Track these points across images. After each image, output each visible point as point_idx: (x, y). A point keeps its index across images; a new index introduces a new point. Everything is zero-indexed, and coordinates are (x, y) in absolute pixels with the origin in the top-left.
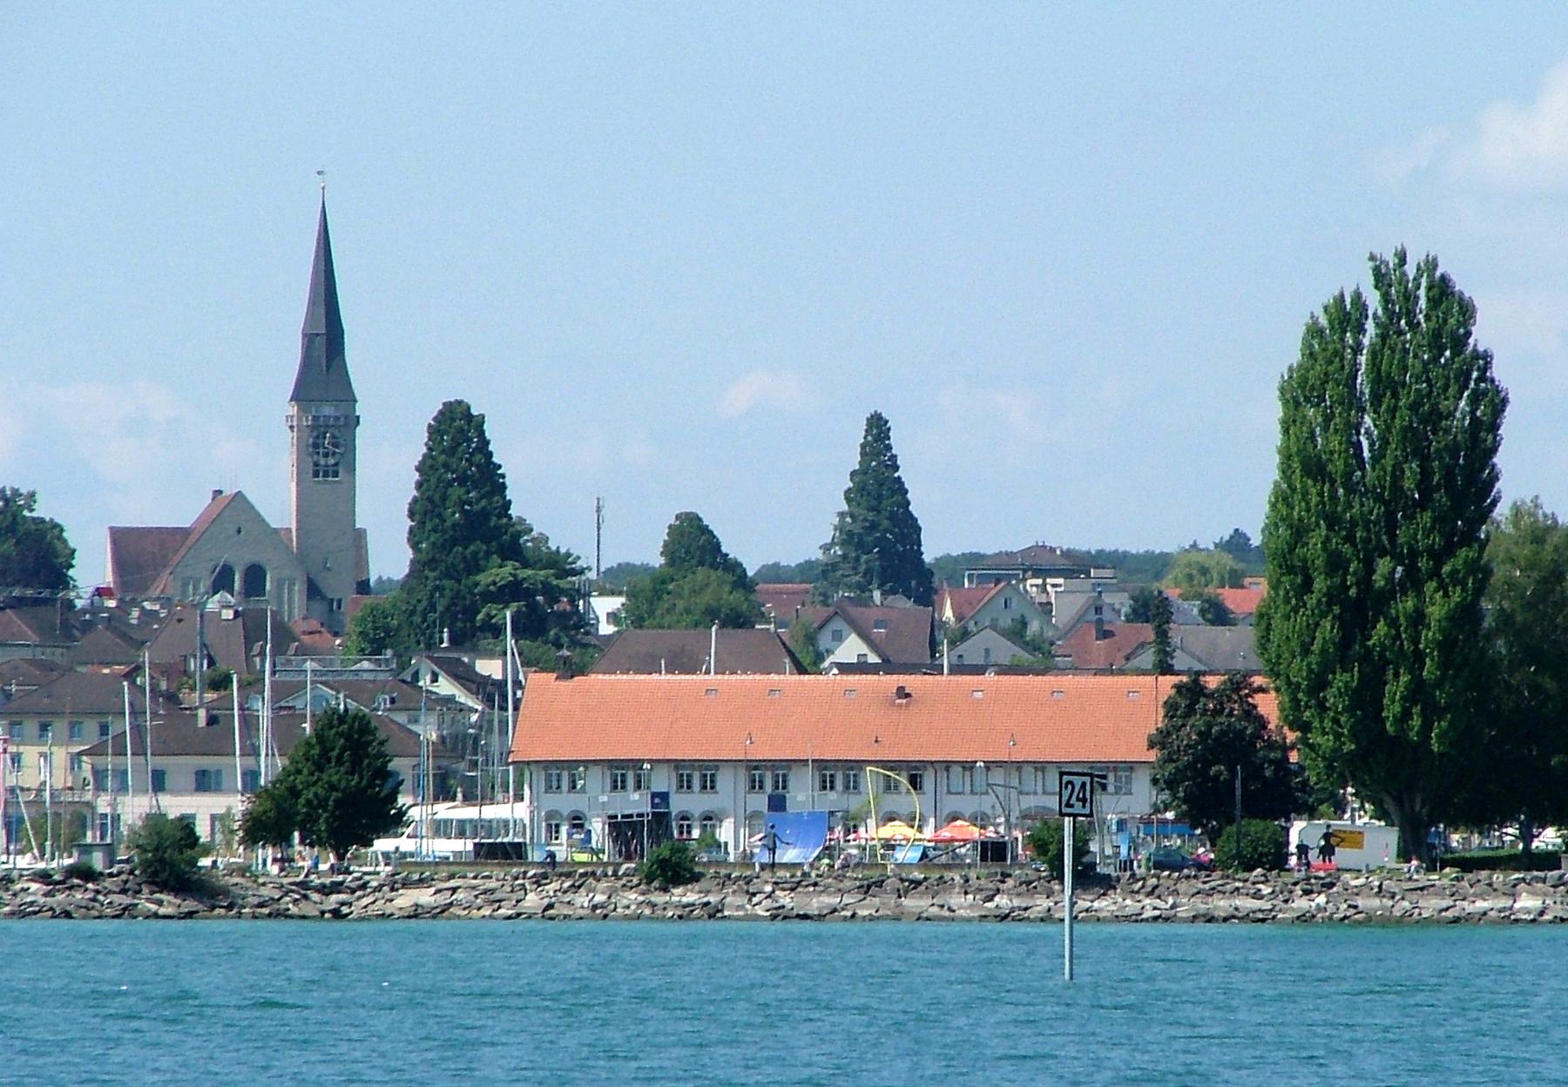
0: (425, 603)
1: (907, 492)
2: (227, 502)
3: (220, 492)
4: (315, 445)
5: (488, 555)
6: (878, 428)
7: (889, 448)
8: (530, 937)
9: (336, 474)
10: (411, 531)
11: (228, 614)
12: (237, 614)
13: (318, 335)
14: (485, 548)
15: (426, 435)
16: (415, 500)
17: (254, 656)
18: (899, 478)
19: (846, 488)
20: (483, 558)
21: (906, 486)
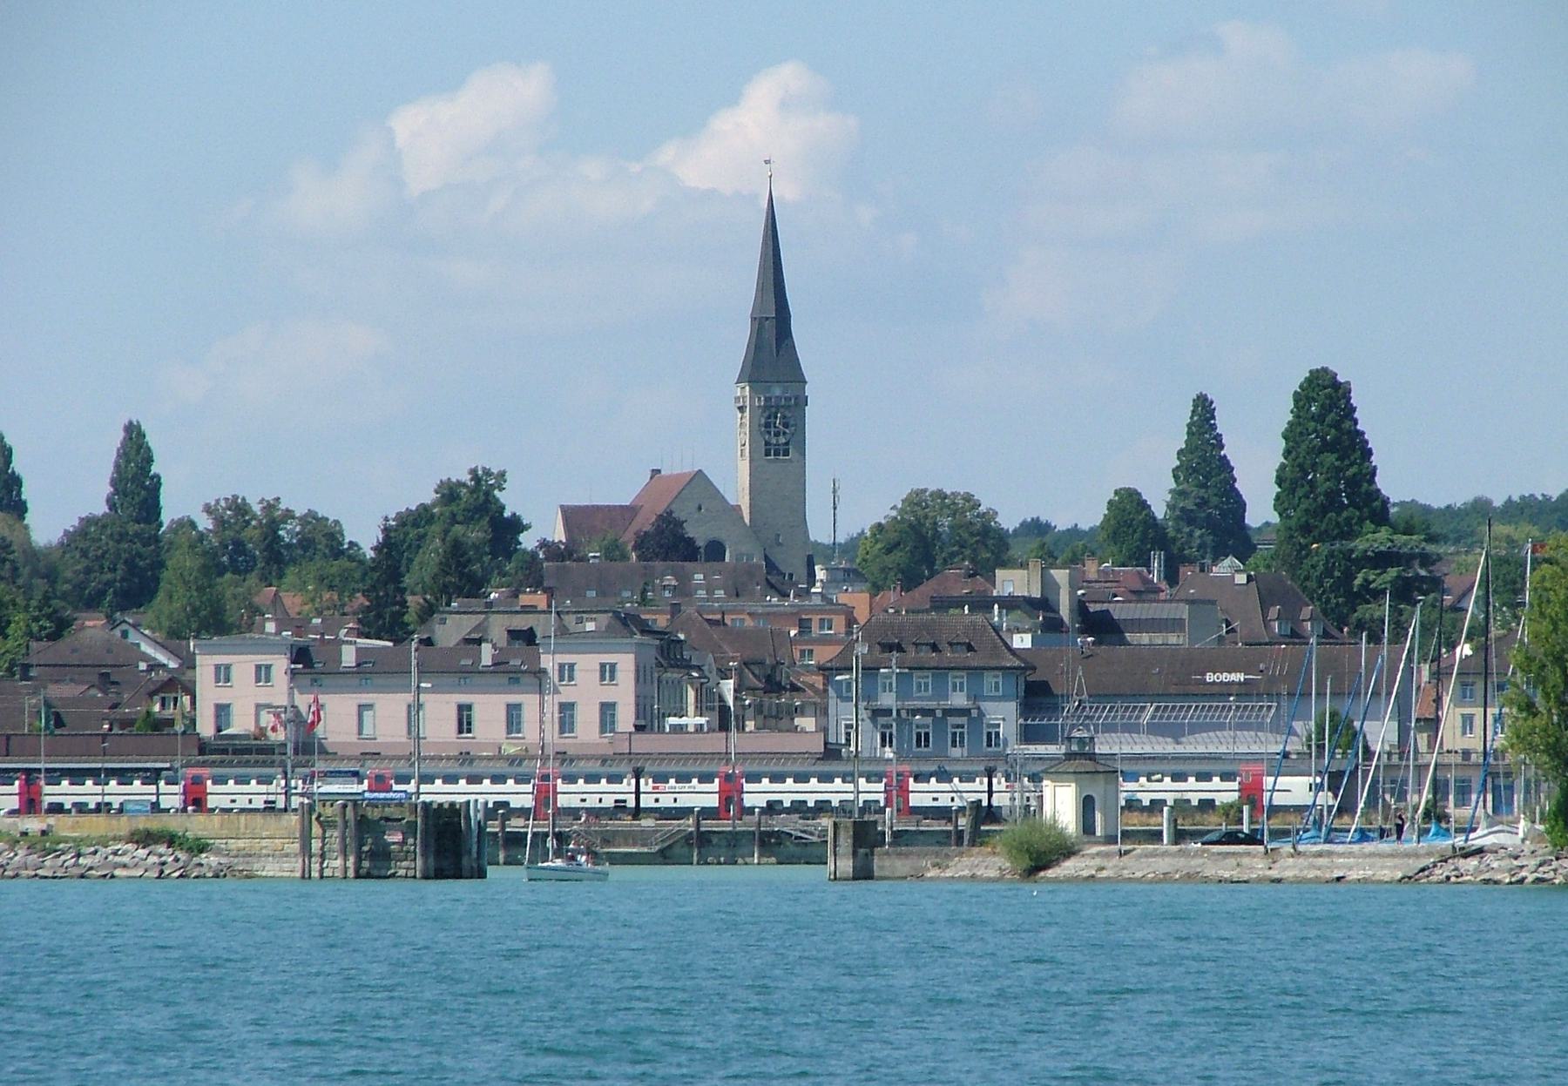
0: (1321, 568)
1: (1233, 469)
2: (688, 479)
3: (659, 471)
4: (767, 425)
5: (1361, 520)
6: (1204, 410)
7: (1214, 427)
8: (561, 891)
9: (786, 453)
10: (1278, 498)
11: (1241, 579)
12: (1249, 578)
13: (767, 319)
14: (1358, 513)
15: (1292, 403)
16: (1282, 467)
17: (1303, 621)
18: (1225, 456)
19: (1174, 466)
20: (1356, 524)
21: (1232, 464)
